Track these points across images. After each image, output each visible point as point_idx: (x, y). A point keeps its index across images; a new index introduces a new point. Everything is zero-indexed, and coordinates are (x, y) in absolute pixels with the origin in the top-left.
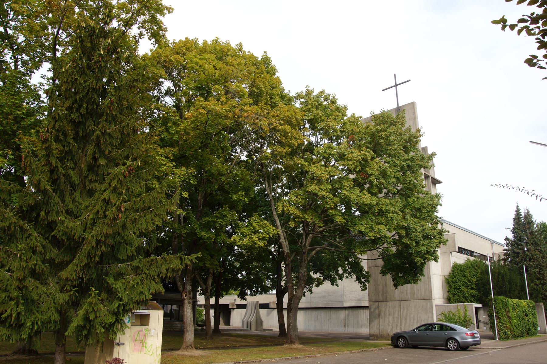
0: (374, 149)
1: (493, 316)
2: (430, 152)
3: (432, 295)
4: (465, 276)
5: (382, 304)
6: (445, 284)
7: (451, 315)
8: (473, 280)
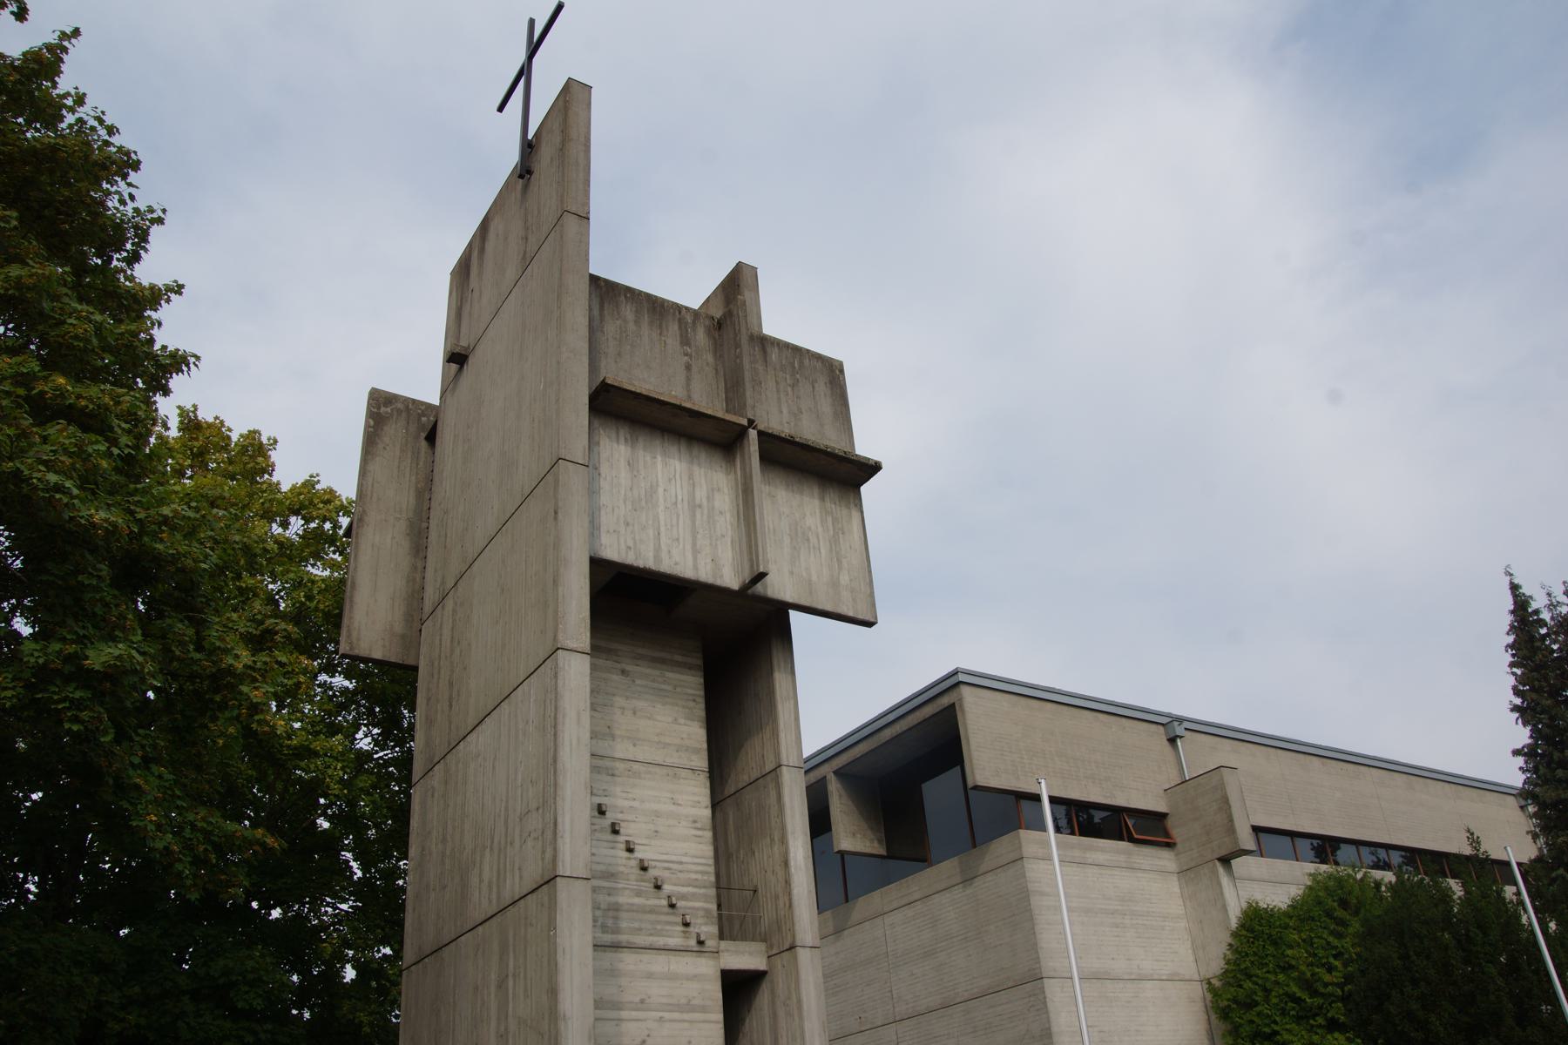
0: (764, 351)
2: (1520, 761)
4: (1287, 968)
8: (1327, 978)
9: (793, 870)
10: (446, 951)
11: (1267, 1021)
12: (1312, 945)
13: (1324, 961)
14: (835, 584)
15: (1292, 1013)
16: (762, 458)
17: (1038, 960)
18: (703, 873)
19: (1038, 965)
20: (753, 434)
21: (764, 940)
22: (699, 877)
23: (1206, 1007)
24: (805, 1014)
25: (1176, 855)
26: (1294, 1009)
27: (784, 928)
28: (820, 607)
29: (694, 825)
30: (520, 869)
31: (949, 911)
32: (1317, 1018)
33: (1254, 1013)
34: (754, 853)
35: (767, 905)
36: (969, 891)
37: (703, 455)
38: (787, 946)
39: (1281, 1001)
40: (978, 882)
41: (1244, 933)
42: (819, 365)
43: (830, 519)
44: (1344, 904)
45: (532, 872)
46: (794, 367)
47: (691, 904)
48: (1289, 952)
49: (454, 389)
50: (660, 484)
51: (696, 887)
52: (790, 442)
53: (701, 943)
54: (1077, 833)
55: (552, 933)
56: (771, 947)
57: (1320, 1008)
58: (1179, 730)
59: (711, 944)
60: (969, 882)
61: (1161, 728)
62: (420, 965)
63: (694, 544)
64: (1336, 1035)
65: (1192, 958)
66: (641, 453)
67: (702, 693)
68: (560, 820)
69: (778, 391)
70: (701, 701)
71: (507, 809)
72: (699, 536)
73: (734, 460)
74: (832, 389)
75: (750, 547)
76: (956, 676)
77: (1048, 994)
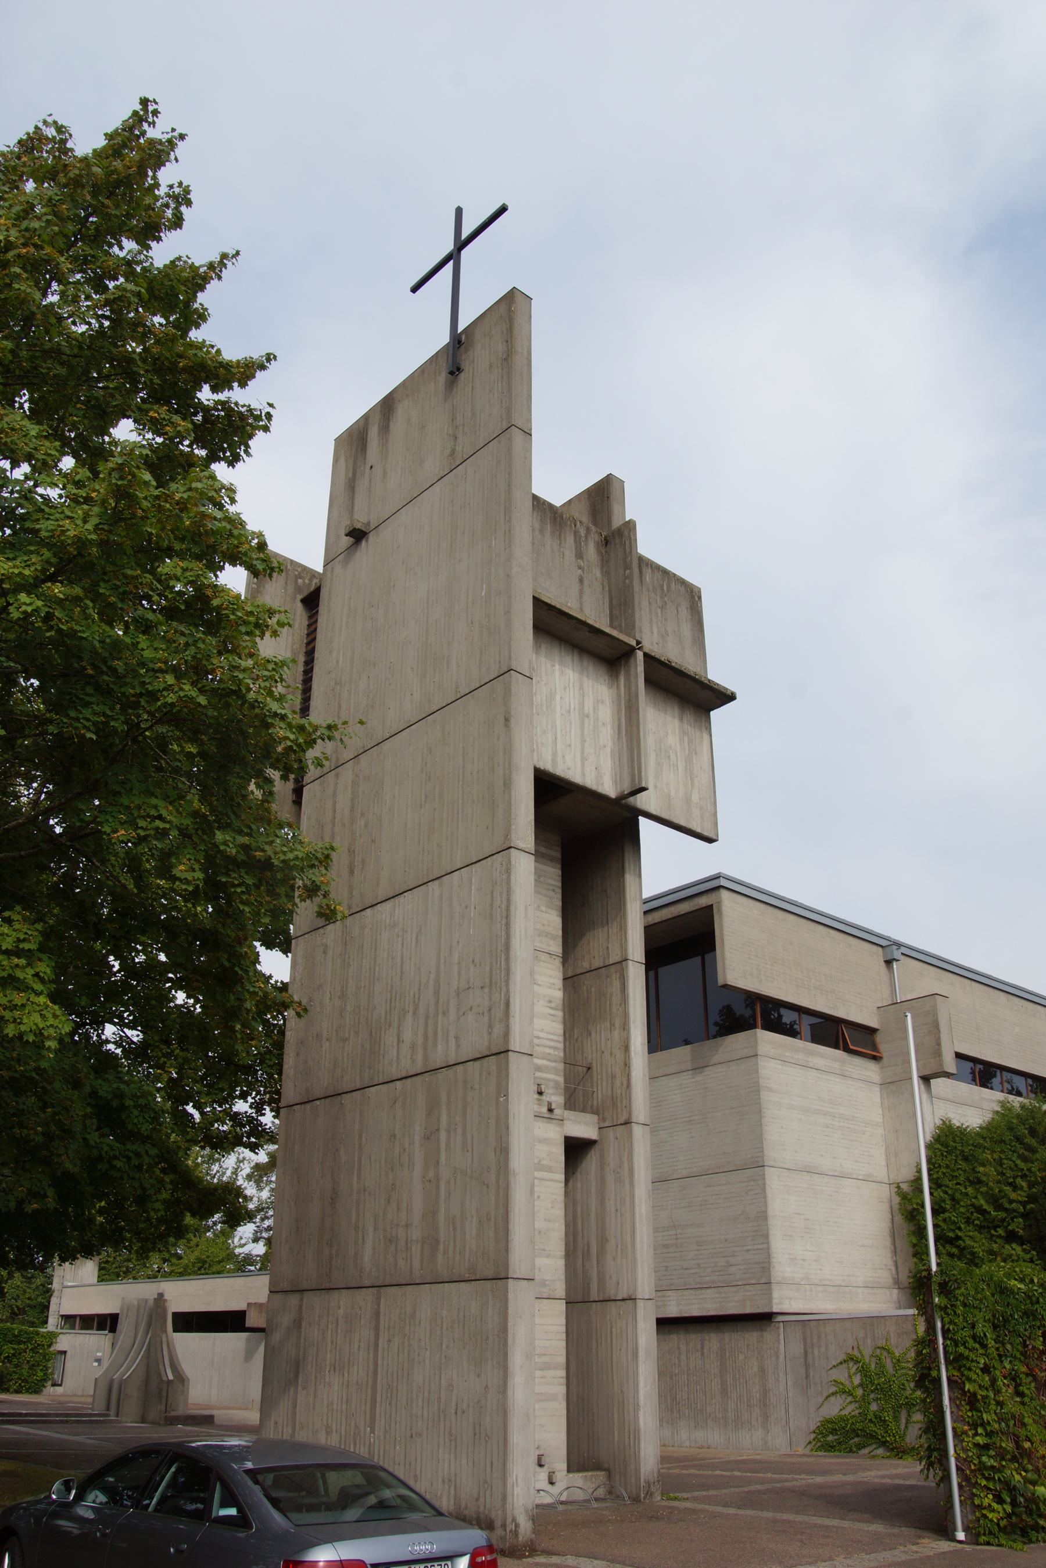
1: (938, 1381)
3: (507, 1250)
5: (315, 1301)
6: (899, 1219)
7: (888, 1364)
8: (1013, 1196)
9: (632, 1054)
10: (347, 1099)
11: (953, 1227)
12: (1001, 1165)
13: (1011, 1180)
14: (688, 801)
15: (976, 1222)
16: (648, 681)
17: (761, 1150)
18: (555, 1048)
19: (760, 1154)
20: (640, 655)
21: (595, 1112)
22: (551, 1051)
23: (891, 1208)
24: (636, 1181)
25: (882, 1068)
26: (978, 1219)
27: (619, 1104)
28: (676, 821)
29: (549, 1005)
30: (457, 1038)
31: (675, 1094)
32: (998, 1229)
33: (940, 1219)
34: (590, 1035)
35: (602, 1083)
36: (699, 1078)
37: (591, 667)
38: (621, 1120)
39: (968, 1211)
40: (708, 1071)
41: (938, 1146)
42: (682, 589)
43: (686, 739)
44: (1033, 1132)
45: (475, 1041)
46: (663, 590)
47: (544, 1075)
48: (981, 1169)
49: (347, 561)
50: (558, 691)
51: (549, 1060)
52: (667, 666)
53: (550, 1110)
54: (841, 1047)
55: (501, 1099)
56: (604, 1120)
57: (1003, 1220)
58: (897, 955)
59: (558, 1112)
60: (700, 1070)
61: (880, 949)
62: (308, 1106)
63: (582, 752)
64: (1014, 1245)
65: (884, 1163)
66: (543, 660)
67: (560, 884)
68: (512, 1001)
69: (650, 612)
70: (559, 891)
71: (437, 981)
72: (587, 744)
73: (617, 677)
74: (692, 615)
75: (632, 762)
76: (717, 880)
77: (768, 1182)
